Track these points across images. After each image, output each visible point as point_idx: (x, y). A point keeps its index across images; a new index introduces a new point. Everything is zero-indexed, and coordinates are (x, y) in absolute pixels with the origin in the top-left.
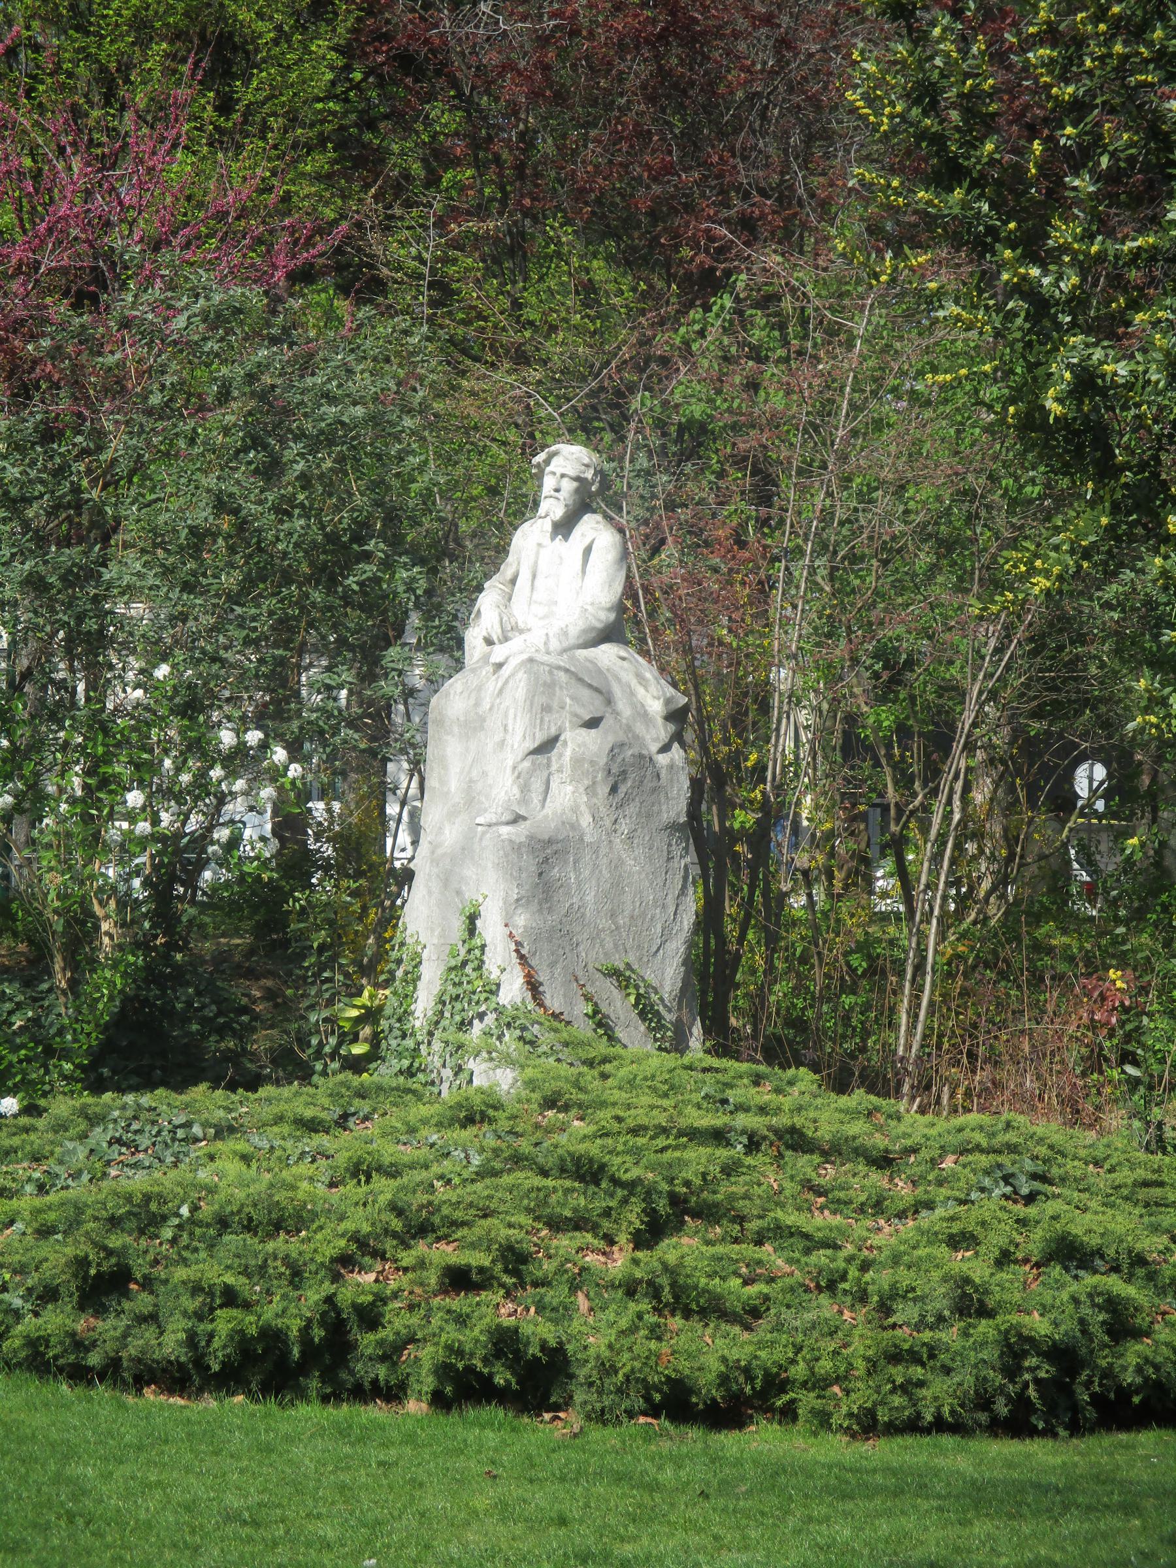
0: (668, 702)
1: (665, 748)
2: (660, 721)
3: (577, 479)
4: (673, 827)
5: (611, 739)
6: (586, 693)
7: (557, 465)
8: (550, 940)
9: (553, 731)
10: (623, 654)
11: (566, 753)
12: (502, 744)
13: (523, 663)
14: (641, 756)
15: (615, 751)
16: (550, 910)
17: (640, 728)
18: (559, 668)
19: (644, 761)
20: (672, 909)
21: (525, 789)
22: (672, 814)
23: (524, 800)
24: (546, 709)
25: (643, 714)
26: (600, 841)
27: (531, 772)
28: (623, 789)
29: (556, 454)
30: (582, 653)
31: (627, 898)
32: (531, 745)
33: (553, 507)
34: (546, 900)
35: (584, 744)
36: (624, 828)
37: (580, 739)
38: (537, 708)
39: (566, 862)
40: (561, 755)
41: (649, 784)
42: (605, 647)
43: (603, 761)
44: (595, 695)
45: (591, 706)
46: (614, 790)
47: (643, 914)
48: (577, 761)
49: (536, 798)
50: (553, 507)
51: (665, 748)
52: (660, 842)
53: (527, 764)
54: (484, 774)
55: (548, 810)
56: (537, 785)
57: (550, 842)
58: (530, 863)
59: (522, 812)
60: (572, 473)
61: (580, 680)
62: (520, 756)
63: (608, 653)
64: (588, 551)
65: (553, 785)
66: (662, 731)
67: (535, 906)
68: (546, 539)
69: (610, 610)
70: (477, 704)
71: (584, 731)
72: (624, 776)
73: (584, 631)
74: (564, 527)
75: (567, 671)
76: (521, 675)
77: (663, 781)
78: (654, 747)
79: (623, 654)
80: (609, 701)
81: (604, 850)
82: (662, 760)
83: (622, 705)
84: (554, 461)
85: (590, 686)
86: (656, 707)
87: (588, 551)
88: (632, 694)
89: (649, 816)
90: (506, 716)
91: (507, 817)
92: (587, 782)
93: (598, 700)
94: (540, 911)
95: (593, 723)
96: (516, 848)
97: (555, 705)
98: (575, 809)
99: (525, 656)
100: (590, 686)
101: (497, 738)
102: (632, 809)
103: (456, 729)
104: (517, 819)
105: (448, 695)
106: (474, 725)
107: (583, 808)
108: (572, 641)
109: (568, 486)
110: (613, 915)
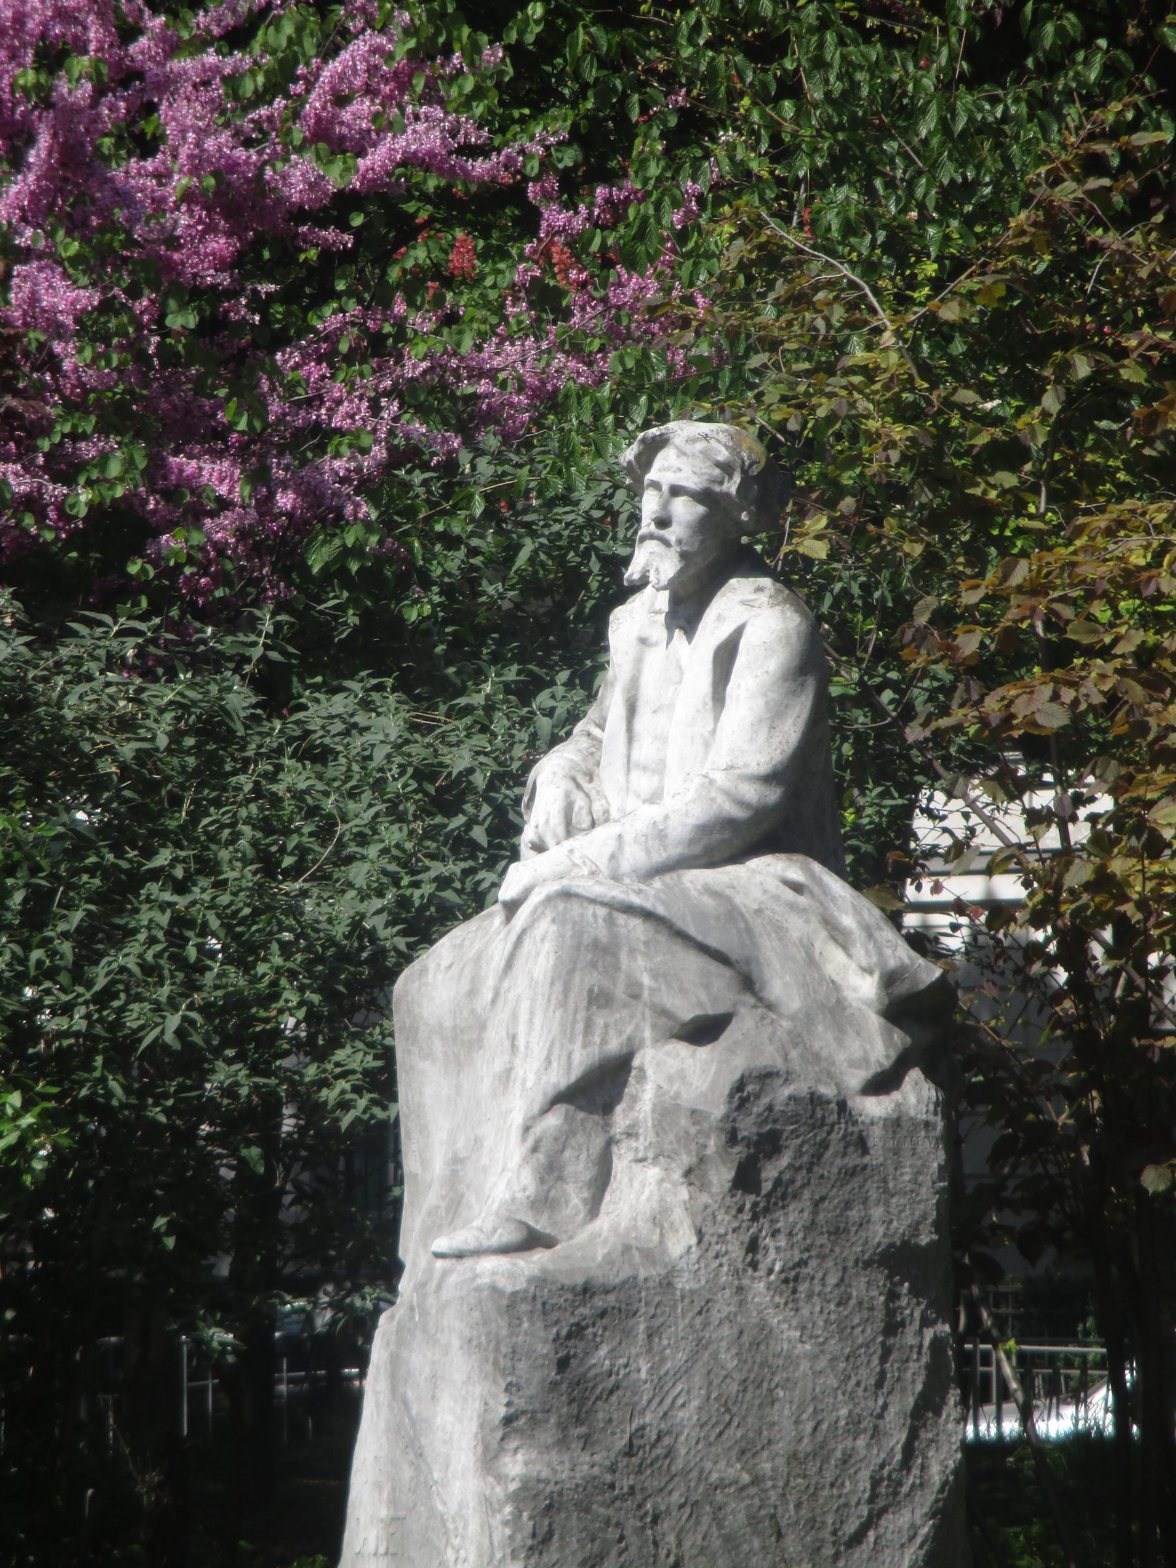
0: (890, 980)
1: (884, 1082)
2: (874, 1021)
3: (704, 496)
4: (898, 1260)
5: (740, 1064)
6: (693, 962)
7: (667, 468)
8: (584, 1508)
9: (614, 1045)
10: (795, 873)
11: (641, 1102)
12: (506, 1076)
13: (549, 900)
14: (815, 1100)
15: (743, 1093)
16: (587, 1442)
17: (823, 1038)
18: (629, 909)
19: (824, 1115)
20: (898, 1438)
21: (551, 1171)
22: (900, 1226)
23: (544, 1202)
24: (599, 999)
25: (835, 1008)
26: (714, 1285)
27: (563, 1140)
28: (769, 1173)
29: (660, 443)
30: (696, 878)
31: (783, 1413)
32: (559, 1078)
33: (655, 562)
34: (578, 1420)
35: (682, 1076)
36: (775, 1256)
37: (673, 1065)
38: (578, 997)
39: (628, 1333)
40: (635, 1099)
41: (832, 1163)
42: (755, 863)
43: (718, 1110)
44: (714, 967)
45: (695, 989)
46: (746, 1179)
47: (821, 1451)
48: (665, 1112)
49: (575, 1197)
50: (655, 562)
51: (884, 1082)
52: (868, 1288)
53: (554, 1120)
54: (478, 1142)
55: (603, 1223)
56: (579, 1167)
57: (586, 1291)
58: (538, 1340)
59: (541, 1225)
60: (692, 481)
61: (681, 936)
62: (539, 1101)
63: (764, 876)
64: (726, 655)
65: (620, 1165)
66: (877, 1045)
67: (548, 1435)
68: (658, 632)
69: (769, 779)
70: (473, 993)
71: (683, 1049)
72: (772, 1150)
73: (704, 829)
74: (686, 610)
75: (647, 915)
76: (545, 926)
77: (876, 1156)
78: (855, 1079)
79: (795, 873)
80: (748, 983)
81: (723, 1306)
82: (875, 1107)
83: (781, 985)
84: (660, 460)
85: (704, 949)
86: (863, 989)
87: (726, 655)
88: (812, 962)
89: (838, 1232)
90: (514, 1016)
91: (508, 1235)
92: (686, 1160)
93: (721, 978)
94: (562, 1443)
95: (704, 1031)
96: (512, 1305)
97: (620, 992)
98: (659, 1219)
99: (555, 887)
100: (704, 949)
101: (498, 1066)
102: (794, 1215)
103: (437, 1046)
104: (532, 1241)
105: (424, 971)
106: (466, 1038)
107: (678, 1214)
108: (675, 851)
109: (685, 511)
110: (746, 1452)
